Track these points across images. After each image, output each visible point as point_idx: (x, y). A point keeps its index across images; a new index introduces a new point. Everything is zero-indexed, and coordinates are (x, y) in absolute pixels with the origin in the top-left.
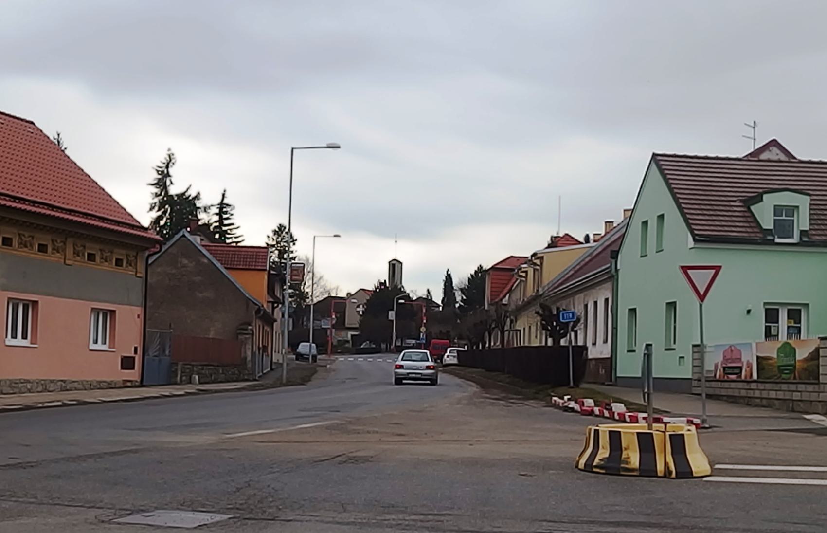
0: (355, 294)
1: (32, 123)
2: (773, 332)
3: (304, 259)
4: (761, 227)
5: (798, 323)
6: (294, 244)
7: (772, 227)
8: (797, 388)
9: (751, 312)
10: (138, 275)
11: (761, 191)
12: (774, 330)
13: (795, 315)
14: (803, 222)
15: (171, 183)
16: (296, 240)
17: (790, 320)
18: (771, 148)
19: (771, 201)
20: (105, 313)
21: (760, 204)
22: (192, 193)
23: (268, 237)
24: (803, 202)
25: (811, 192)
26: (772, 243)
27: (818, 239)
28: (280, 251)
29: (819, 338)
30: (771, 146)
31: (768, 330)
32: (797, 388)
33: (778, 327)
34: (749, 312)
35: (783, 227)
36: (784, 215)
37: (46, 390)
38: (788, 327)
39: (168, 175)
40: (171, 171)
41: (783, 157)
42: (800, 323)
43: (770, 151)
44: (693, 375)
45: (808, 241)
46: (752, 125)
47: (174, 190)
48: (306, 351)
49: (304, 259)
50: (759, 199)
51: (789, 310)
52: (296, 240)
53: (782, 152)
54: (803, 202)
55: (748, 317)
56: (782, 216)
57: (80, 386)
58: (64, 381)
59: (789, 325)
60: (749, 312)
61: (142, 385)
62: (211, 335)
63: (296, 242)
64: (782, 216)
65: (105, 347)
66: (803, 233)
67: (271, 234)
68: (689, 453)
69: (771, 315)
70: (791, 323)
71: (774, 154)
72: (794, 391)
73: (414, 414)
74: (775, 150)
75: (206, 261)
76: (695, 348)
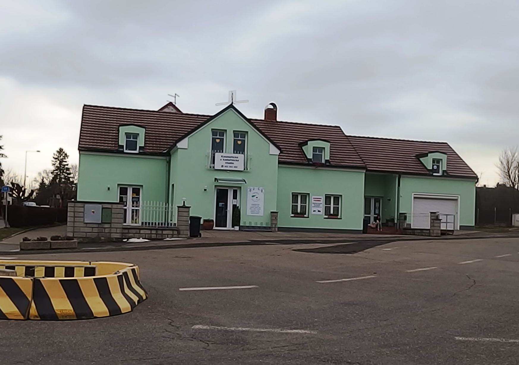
1: (446, 143)
2: (124, 200)
3: (75, 165)
4: (306, 157)
5: (121, 197)
6: (68, 158)
7: (311, 157)
8: (128, 231)
9: (110, 189)
11: (307, 140)
12: (125, 199)
13: (136, 191)
14: (141, 142)
16: (68, 156)
17: (133, 194)
18: (169, 107)
19: (431, 156)
21: (427, 158)
23: (54, 154)
24: (141, 132)
25: (146, 127)
26: (123, 152)
27: (148, 151)
28: (60, 161)
29: (430, 212)
30: (169, 106)
32: (128, 231)
33: (127, 197)
34: (109, 189)
35: (132, 145)
36: (132, 138)
38: (133, 198)
42: (139, 195)
43: (168, 108)
44: (431, 227)
45: (144, 153)
46: (174, 95)
48: (249, 213)
49: (75, 165)
50: (306, 143)
51: (133, 189)
52: (68, 156)
53: (175, 108)
54: (141, 132)
55: (109, 191)
56: (130, 138)
59: (133, 196)
60: (109, 189)
61: (364, 233)
63: (69, 157)
64: (130, 138)
67: (56, 153)
70: (134, 195)
71: (171, 109)
72: (136, 233)
73: (65, 247)
74: (171, 107)
76: (272, 214)
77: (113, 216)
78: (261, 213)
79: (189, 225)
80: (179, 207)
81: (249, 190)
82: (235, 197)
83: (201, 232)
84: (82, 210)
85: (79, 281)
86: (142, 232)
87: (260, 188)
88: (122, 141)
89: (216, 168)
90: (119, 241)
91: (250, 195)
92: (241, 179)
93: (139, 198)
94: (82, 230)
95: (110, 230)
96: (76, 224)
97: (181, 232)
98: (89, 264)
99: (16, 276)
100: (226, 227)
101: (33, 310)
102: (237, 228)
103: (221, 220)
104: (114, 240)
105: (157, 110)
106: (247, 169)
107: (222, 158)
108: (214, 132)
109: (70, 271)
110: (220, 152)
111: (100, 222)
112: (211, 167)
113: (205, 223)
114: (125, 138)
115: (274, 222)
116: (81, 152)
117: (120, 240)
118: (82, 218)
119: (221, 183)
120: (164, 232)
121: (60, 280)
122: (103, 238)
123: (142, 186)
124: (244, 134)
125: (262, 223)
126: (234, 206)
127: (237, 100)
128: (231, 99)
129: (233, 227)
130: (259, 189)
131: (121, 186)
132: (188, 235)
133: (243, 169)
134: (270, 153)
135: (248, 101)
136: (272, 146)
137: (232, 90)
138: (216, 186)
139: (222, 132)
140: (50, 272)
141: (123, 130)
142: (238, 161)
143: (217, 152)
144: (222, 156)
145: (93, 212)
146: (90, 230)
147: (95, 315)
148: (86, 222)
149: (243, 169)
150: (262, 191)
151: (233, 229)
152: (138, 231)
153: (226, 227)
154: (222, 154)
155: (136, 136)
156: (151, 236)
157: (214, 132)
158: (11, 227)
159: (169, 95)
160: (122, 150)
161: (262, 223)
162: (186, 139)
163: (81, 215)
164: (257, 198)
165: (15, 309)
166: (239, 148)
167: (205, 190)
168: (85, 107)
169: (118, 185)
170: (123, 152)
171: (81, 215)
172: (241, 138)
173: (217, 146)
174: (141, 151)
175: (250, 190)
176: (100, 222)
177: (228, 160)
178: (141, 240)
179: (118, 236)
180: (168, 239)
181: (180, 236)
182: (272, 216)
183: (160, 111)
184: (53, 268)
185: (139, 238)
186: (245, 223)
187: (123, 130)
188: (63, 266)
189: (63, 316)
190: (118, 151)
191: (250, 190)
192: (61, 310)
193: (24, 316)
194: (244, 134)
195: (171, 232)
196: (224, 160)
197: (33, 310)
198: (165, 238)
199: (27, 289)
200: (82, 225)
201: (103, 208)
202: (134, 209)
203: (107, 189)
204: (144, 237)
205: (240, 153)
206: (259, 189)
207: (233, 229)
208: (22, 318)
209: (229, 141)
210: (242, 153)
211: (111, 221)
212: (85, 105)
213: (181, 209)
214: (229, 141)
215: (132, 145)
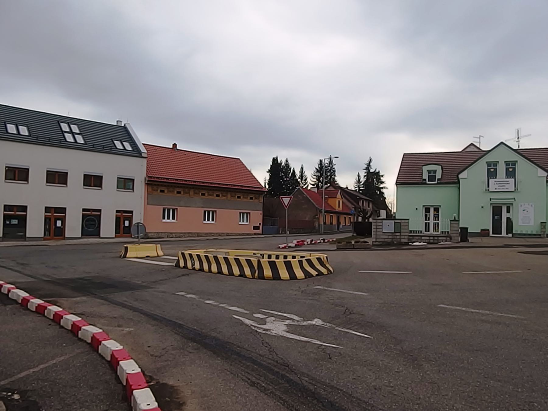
0: (328, 204)
9: (418, 209)
10: (260, 201)
13: (437, 210)
14: (439, 176)
15: (371, 168)
20: (247, 213)
22: (377, 171)
24: (439, 169)
26: (426, 184)
31: (426, 216)
34: (417, 209)
35: (432, 178)
37: (220, 236)
38: (434, 215)
39: (370, 166)
40: (371, 164)
41: (477, 150)
45: (441, 183)
47: (372, 171)
48: (520, 223)
55: (417, 211)
57: (235, 234)
58: (228, 233)
60: (417, 209)
62: (307, 219)
65: (247, 223)
66: (438, 179)
68: (129, 251)
69: (427, 210)
71: (472, 149)
74: (472, 147)
75: (305, 196)
77: (402, 227)
78: (532, 223)
79: (458, 233)
80: (451, 221)
81: (520, 205)
82: (508, 211)
83: (468, 238)
84: (381, 224)
85: (276, 262)
86: (423, 238)
87: (530, 204)
88: (425, 176)
89: (490, 190)
90: (407, 244)
91: (521, 209)
92: (512, 197)
93: (438, 215)
94: (382, 237)
95: (400, 237)
96: (378, 233)
97: (453, 238)
98: (309, 256)
99: (229, 256)
100: (501, 234)
101: (256, 274)
102: (510, 235)
103: (497, 229)
104: (403, 243)
105: (460, 150)
106: (517, 190)
107: (495, 183)
108: (489, 164)
109: (285, 257)
110: (493, 178)
111: (393, 232)
112: (486, 190)
113: (483, 232)
114: (427, 173)
115: (544, 230)
116: (398, 186)
117: (407, 243)
118: (381, 230)
119: (493, 201)
120: (440, 238)
121: (246, 260)
122: (395, 242)
123: (440, 206)
124: (514, 163)
125: (537, 232)
126: (509, 220)
127: (522, 135)
128: (517, 135)
129: (507, 234)
130: (529, 205)
131: (435, 207)
132: (458, 240)
133: (513, 190)
134: (539, 175)
135: (531, 135)
136: (540, 170)
137: (517, 128)
138: (491, 204)
139: (496, 164)
140: (262, 255)
141: (425, 169)
142: (509, 184)
143: (491, 178)
144: (495, 181)
145: (389, 225)
146: (386, 237)
147: (282, 278)
148: (384, 231)
149: (513, 190)
150: (532, 206)
151: (507, 236)
152: (420, 237)
153: (501, 234)
154: (495, 180)
155: (435, 172)
156: (430, 241)
157: (489, 164)
158: (357, 235)
159: (474, 137)
160: (425, 182)
161: (537, 232)
162: (466, 171)
163: (380, 227)
164: (527, 211)
165: (250, 273)
166: (511, 173)
167: (482, 207)
168: (405, 155)
169: (424, 206)
170: (426, 184)
171: (380, 227)
172: (512, 166)
173: (492, 174)
174: (439, 182)
175: (521, 206)
176: (393, 232)
177: (499, 183)
178: (422, 244)
179: (406, 241)
180: (442, 243)
181: (452, 241)
182: (542, 225)
183: (464, 151)
184: (279, 256)
185: (420, 242)
186: (516, 231)
187: (425, 169)
188: (282, 255)
189: (267, 278)
190: (423, 183)
191: (521, 206)
192: (267, 275)
193: (252, 276)
194: (514, 163)
195: (445, 238)
196: (497, 184)
197: (256, 274)
198: (440, 243)
199: (255, 265)
200: (382, 234)
201: (395, 223)
202: (436, 223)
203: (415, 209)
204: (424, 241)
205: (510, 178)
206: (529, 205)
207: (507, 236)
208: (251, 277)
209: (501, 170)
210: (513, 178)
211: (401, 230)
212: (404, 154)
213: (452, 222)
214: (501, 170)
215: (432, 178)
